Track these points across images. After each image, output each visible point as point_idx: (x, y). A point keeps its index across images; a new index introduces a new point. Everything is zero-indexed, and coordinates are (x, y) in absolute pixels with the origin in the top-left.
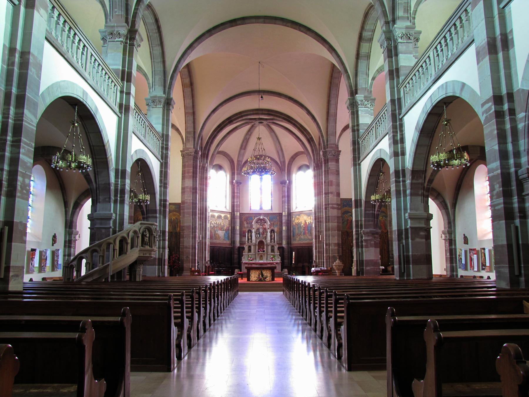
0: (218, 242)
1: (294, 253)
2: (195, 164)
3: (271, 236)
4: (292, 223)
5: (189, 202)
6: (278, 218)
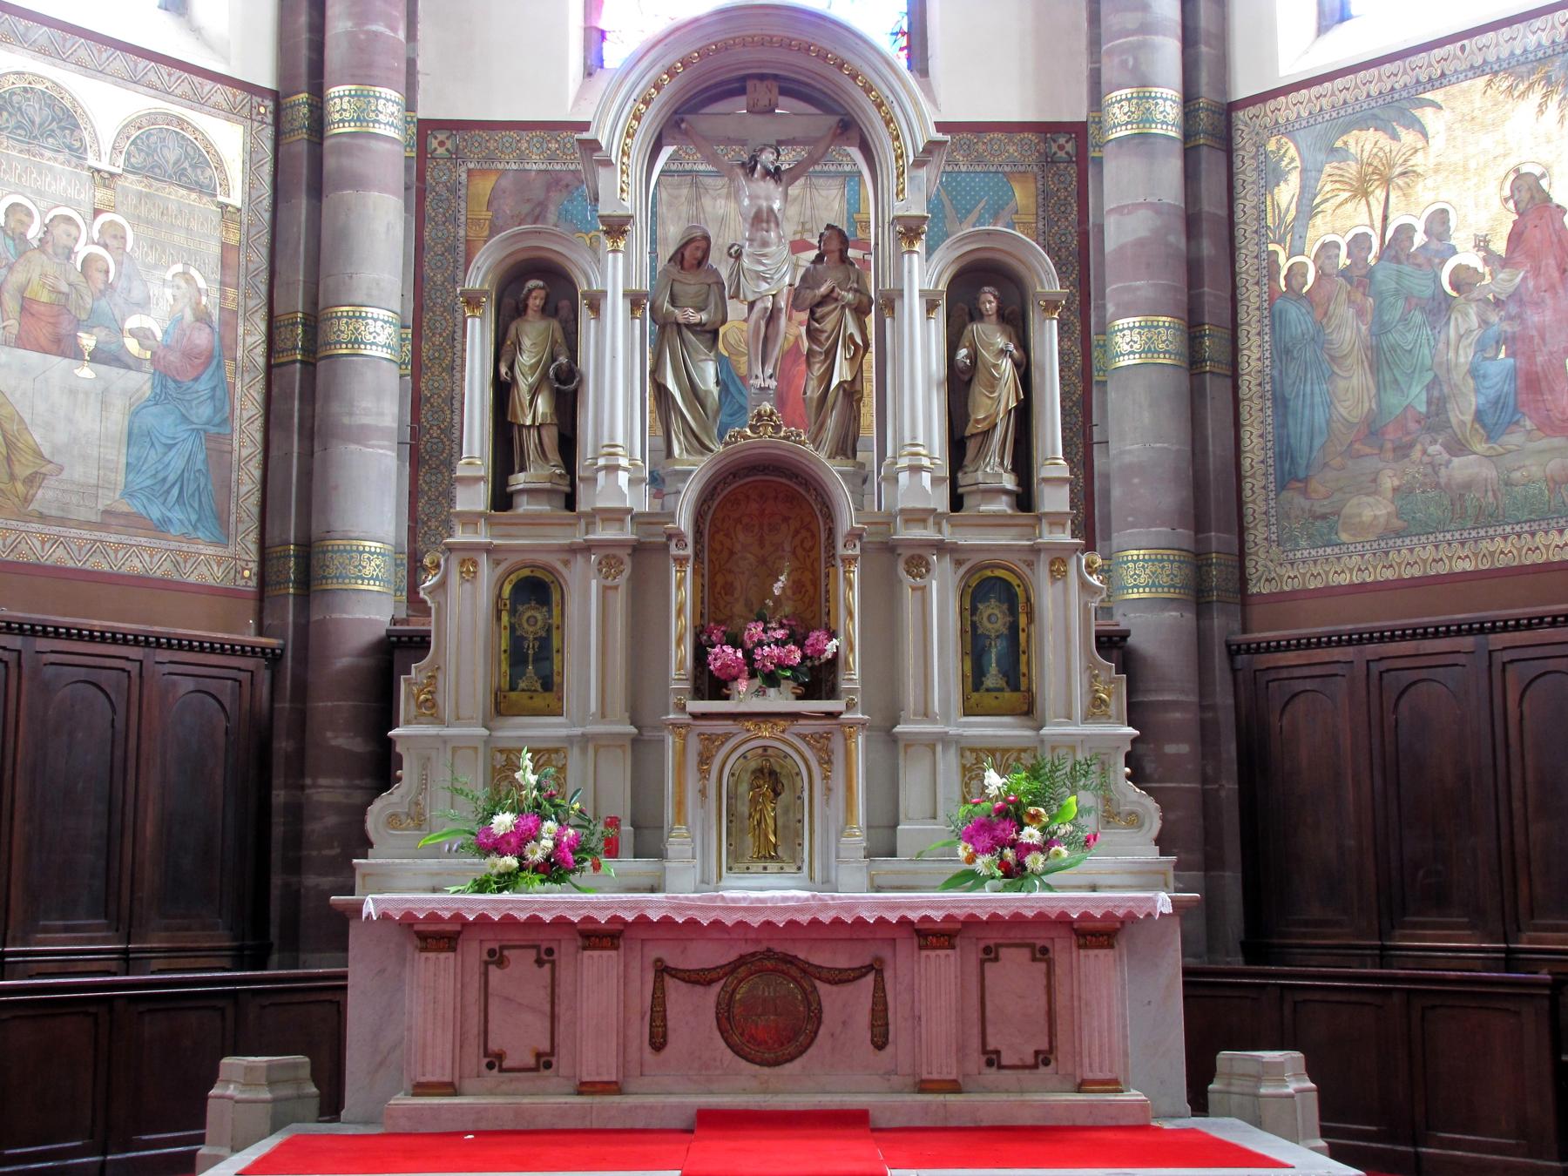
1: (7, 1152)
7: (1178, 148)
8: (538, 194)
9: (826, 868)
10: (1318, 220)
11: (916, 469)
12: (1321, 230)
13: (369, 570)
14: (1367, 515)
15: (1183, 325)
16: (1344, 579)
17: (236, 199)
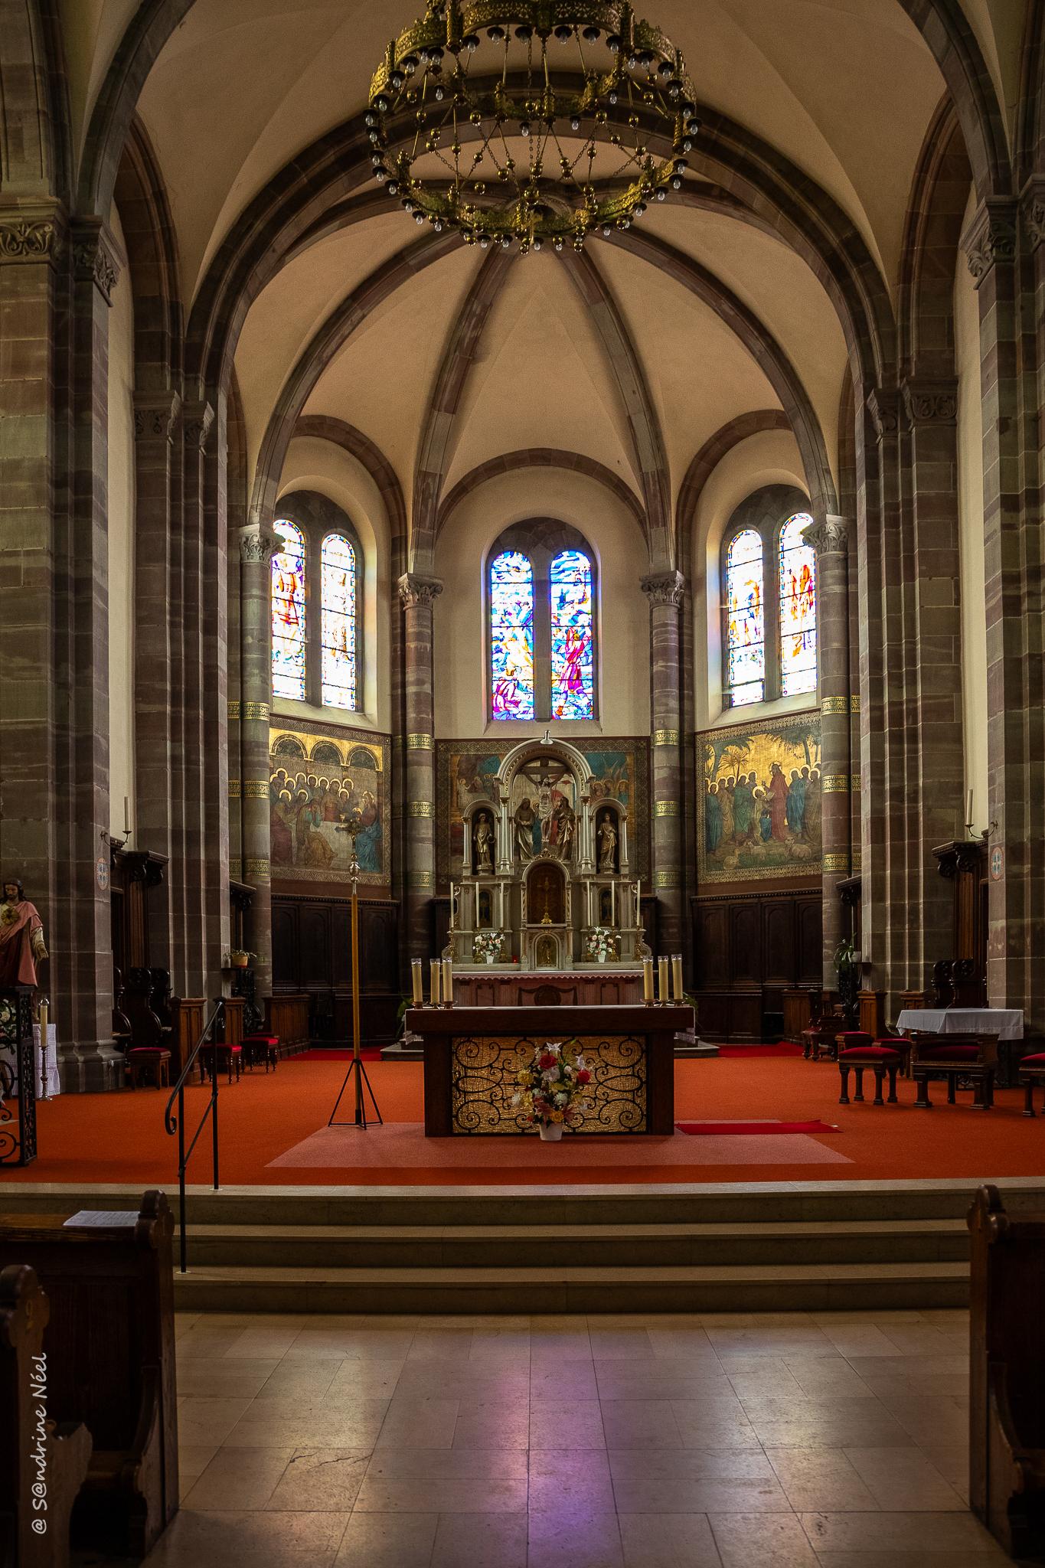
0: (321, 879)
2: (70, 314)
3: (599, 840)
4: (699, 784)
5: (28, 571)
6: (629, 760)
7: (677, 748)
8: (473, 761)
9: (562, 965)
10: (719, 772)
11: (586, 864)
12: (720, 775)
13: (426, 880)
14: (731, 862)
15: (678, 803)
16: (724, 880)
17: (381, 769)
